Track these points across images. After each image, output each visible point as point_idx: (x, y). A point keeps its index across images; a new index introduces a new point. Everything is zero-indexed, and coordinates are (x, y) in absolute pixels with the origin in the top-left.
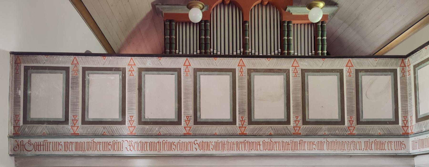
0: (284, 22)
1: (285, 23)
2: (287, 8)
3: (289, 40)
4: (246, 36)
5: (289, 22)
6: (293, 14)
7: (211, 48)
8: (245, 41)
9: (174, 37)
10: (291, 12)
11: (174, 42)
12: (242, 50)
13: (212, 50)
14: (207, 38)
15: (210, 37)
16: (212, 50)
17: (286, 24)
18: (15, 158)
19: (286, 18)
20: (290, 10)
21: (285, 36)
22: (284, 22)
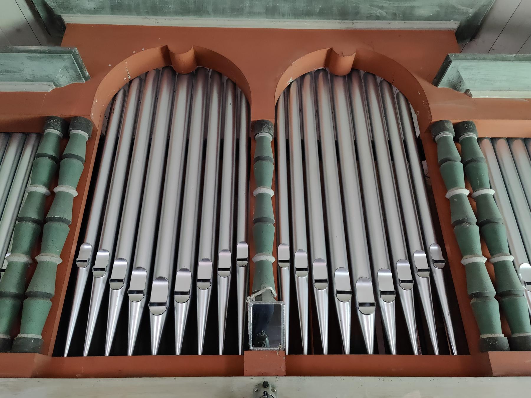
0: (440, 126)
1: (444, 129)
2: (447, 63)
3: (481, 205)
4: (261, 184)
5: (461, 129)
6: (476, 94)
7: (278, 241)
8: (254, 201)
9: (272, 193)
10: (467, 85)
11: (270, 213)
12: (243, 249)
13: (284, 251)
14: (261, 196)
15: (276, 187)
16: (284, 251)
17: (450, 135)
18: (28, 24)
19: (444, 109)
20: (464, 75)
21: (455, 184)
22: (440, 126)
